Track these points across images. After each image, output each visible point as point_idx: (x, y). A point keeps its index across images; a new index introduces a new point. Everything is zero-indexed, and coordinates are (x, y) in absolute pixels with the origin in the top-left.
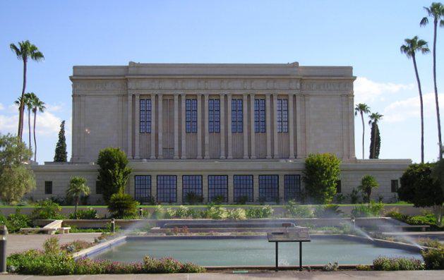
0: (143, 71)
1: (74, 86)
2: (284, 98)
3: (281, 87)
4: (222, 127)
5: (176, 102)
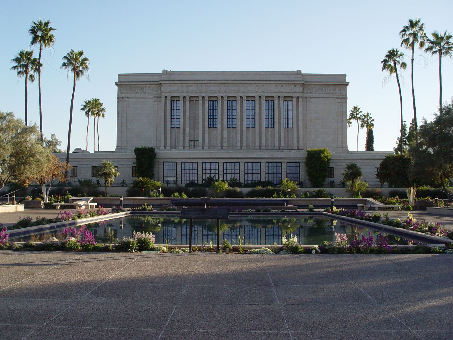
0: (174, 77)
1: (119, 90)
2: (288, 99)
3: (288, 90)
4: (238, 123)
5: (200, 102)
